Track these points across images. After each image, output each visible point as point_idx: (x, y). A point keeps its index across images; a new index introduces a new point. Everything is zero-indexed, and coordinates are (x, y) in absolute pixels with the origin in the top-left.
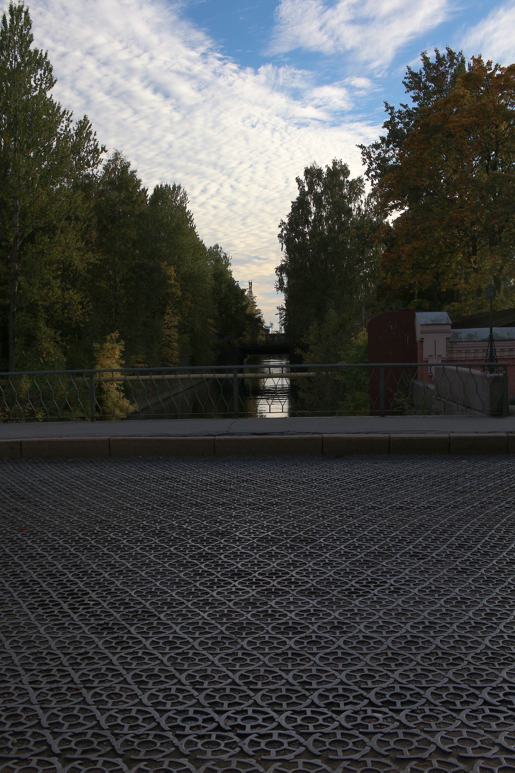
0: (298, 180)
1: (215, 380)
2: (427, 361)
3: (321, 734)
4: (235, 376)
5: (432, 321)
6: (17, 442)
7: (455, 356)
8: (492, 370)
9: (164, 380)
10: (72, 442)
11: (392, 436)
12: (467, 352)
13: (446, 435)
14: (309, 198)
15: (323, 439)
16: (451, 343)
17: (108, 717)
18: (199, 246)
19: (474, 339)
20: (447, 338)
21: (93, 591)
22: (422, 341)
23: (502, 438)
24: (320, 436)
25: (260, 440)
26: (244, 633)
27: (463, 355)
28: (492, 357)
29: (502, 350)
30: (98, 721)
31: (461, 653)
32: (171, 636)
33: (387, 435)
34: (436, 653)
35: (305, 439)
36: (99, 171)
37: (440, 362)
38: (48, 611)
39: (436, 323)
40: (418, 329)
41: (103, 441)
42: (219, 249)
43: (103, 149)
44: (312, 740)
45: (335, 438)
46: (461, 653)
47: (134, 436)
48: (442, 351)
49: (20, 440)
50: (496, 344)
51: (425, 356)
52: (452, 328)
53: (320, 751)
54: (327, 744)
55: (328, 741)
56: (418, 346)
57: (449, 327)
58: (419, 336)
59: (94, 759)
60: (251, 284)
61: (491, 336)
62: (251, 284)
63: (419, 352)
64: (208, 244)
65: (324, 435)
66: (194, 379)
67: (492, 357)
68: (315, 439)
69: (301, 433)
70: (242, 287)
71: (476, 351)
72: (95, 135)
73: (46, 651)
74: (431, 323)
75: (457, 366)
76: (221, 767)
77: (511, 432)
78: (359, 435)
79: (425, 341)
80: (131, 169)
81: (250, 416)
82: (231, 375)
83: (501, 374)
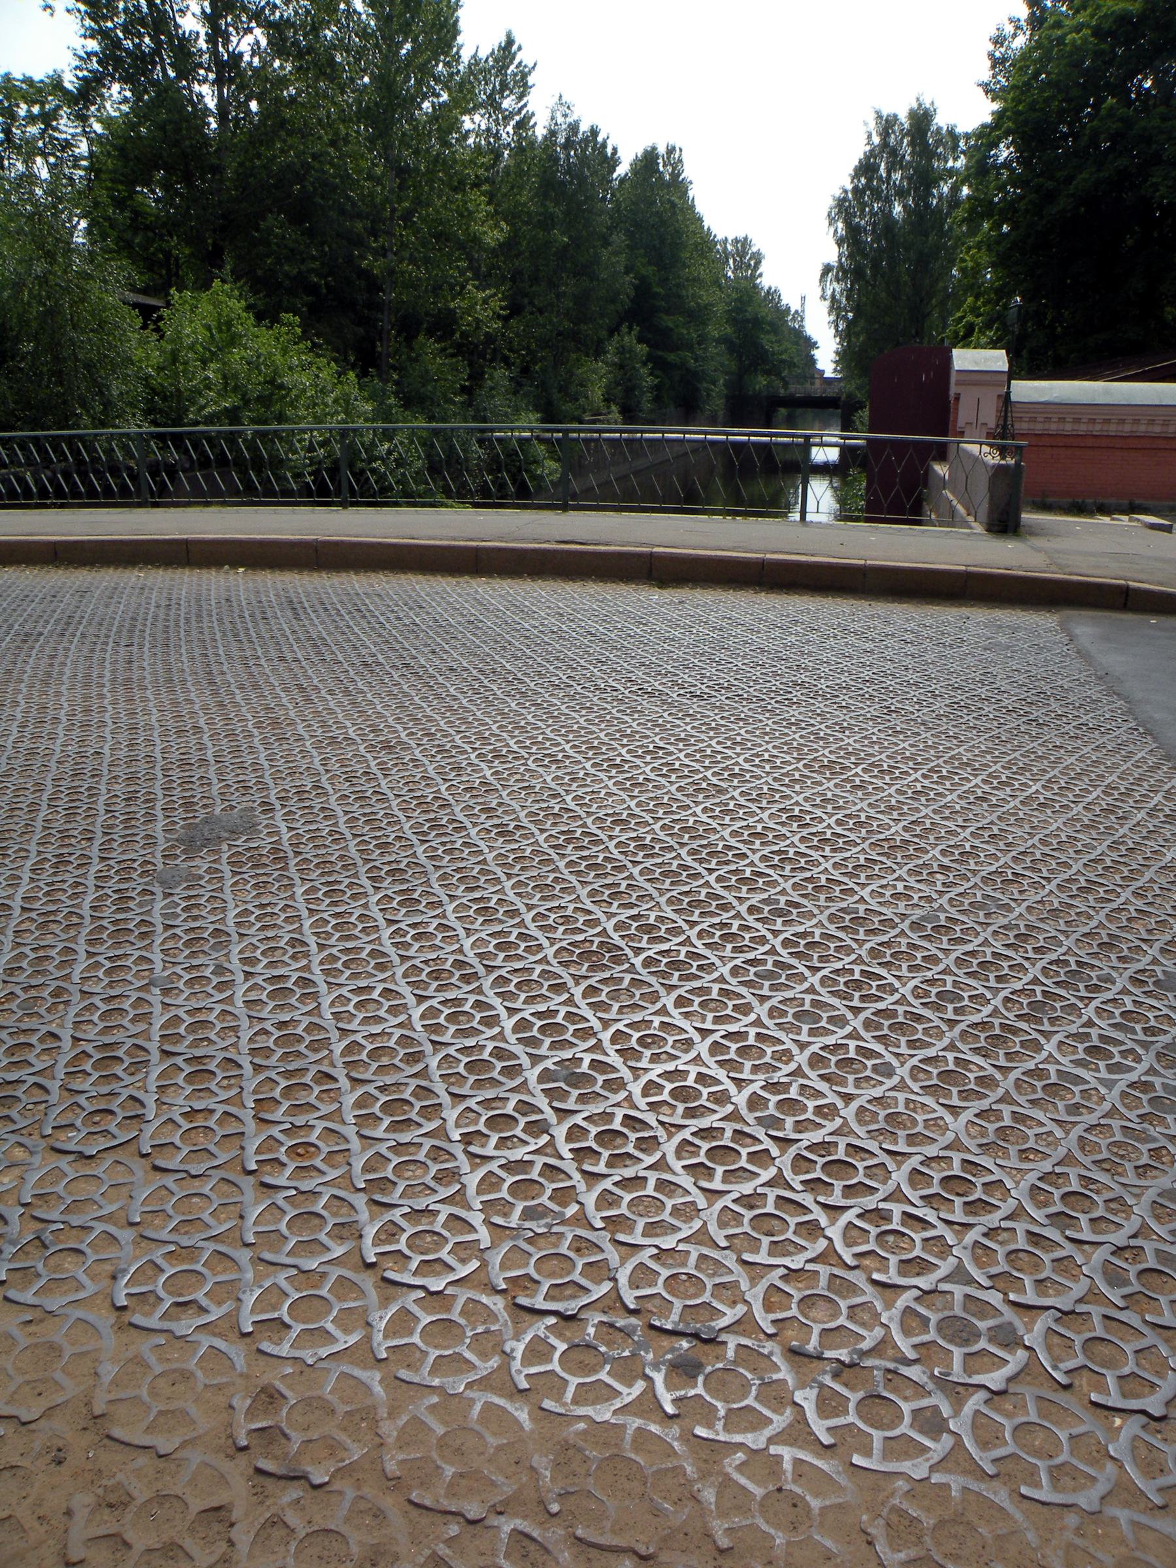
22: (957, 399)
51: (961, 422)
58: (953, 390)
60: (803, 298)
62: (803, 298)
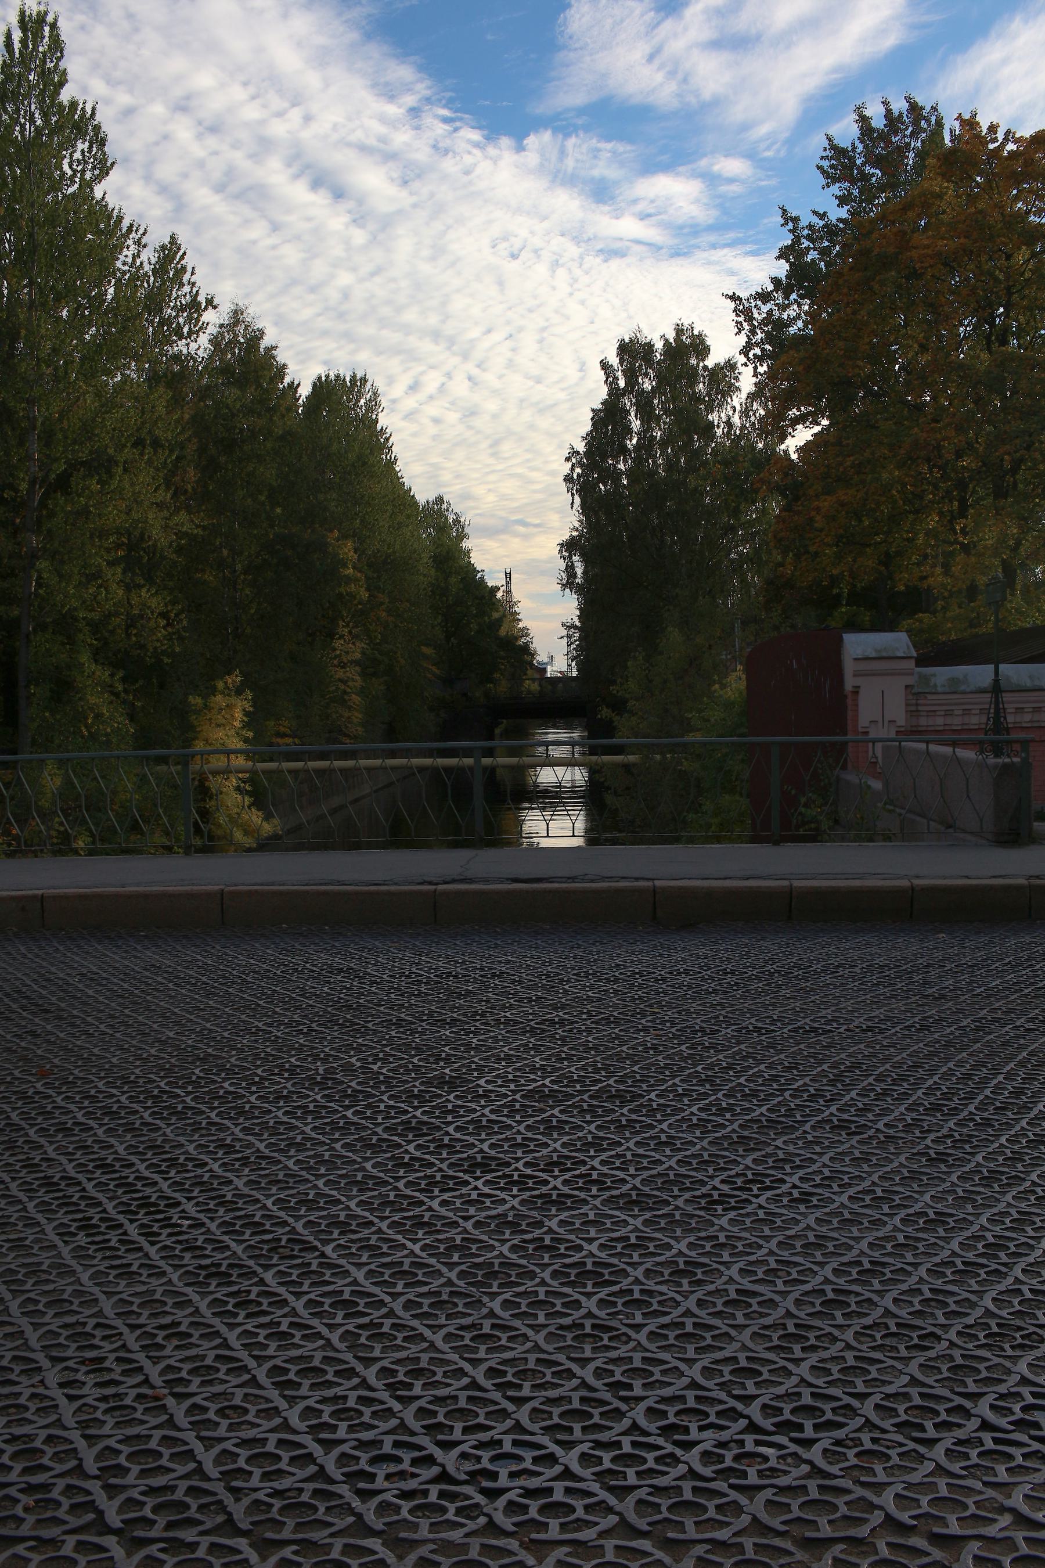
0: (605, 366)
1: (435, 771)
2: (866, 733)
3: (651, 1490)
4: (478, 762)
5: (876, 651)
6: (35, 897)
7: (923, 721)
8: (998, 750)
9: (332, 770)
10: (146, 896)
11: (796, 883)
12: (948, 714)
13: (905, 883)
14: (627, 402)
15: (655, 891)
16: (915, 696)
17: (219, 1455)
18: (403, 498)
19: (963, 688)
20: (907, 687)
21: (189, 1199)
22: (856, 691)
23: (1019, 888)
24: (650, 884)
25: (527, 892)
26: (495, 1284)
27: (940, 721)
28: (998, 725)
29: (1019, 710)
30: (200, 1463)
31: (935, 1325)
32: (347, 1290)
33: (786, 883)
34: (886, 1324)
35: (618, 891)
36: (201, 346)
37: (893, 735)
38: (97, 1239)
39: (884, 654)
40: (849, 667)
41: (209, 895)
42: (444, 506)
43: (210, 302)
44: (634, 1501)
45: (680, 888)
46: (935, 1325)
47: (273, 884)
48: (897, 712)
49: (40, 892)
50: (1007, 697)
51: (863, 721)
52: (917, 666)
53: (649, 1524)
54: (664, 1509)
55: (665, 1503)
56: (849, 701)
57: (912, 664)
58: (850, 682)
59: (190, 1539)
60: (508, 575)
61: (996, 681)
62: (508, 575)
63: (850, 714)
64: (423, 494)
65: (658, 883)
66: (394, 768)
67: (998, 725)
68: (639, 891)
69: (610, 878)
70: (491, 583)
71: (966, 712)
72: (193, 274)
73: (92, 1322)
74: (874, 655)
75: (928, 742)
76: (449, 1556)
77: (1038, 877)
78: (728, 883)
79: (862, 691)
80: (265, 343)
81: (508, 843)
82: (469, 761)
83: (1016, 760)
